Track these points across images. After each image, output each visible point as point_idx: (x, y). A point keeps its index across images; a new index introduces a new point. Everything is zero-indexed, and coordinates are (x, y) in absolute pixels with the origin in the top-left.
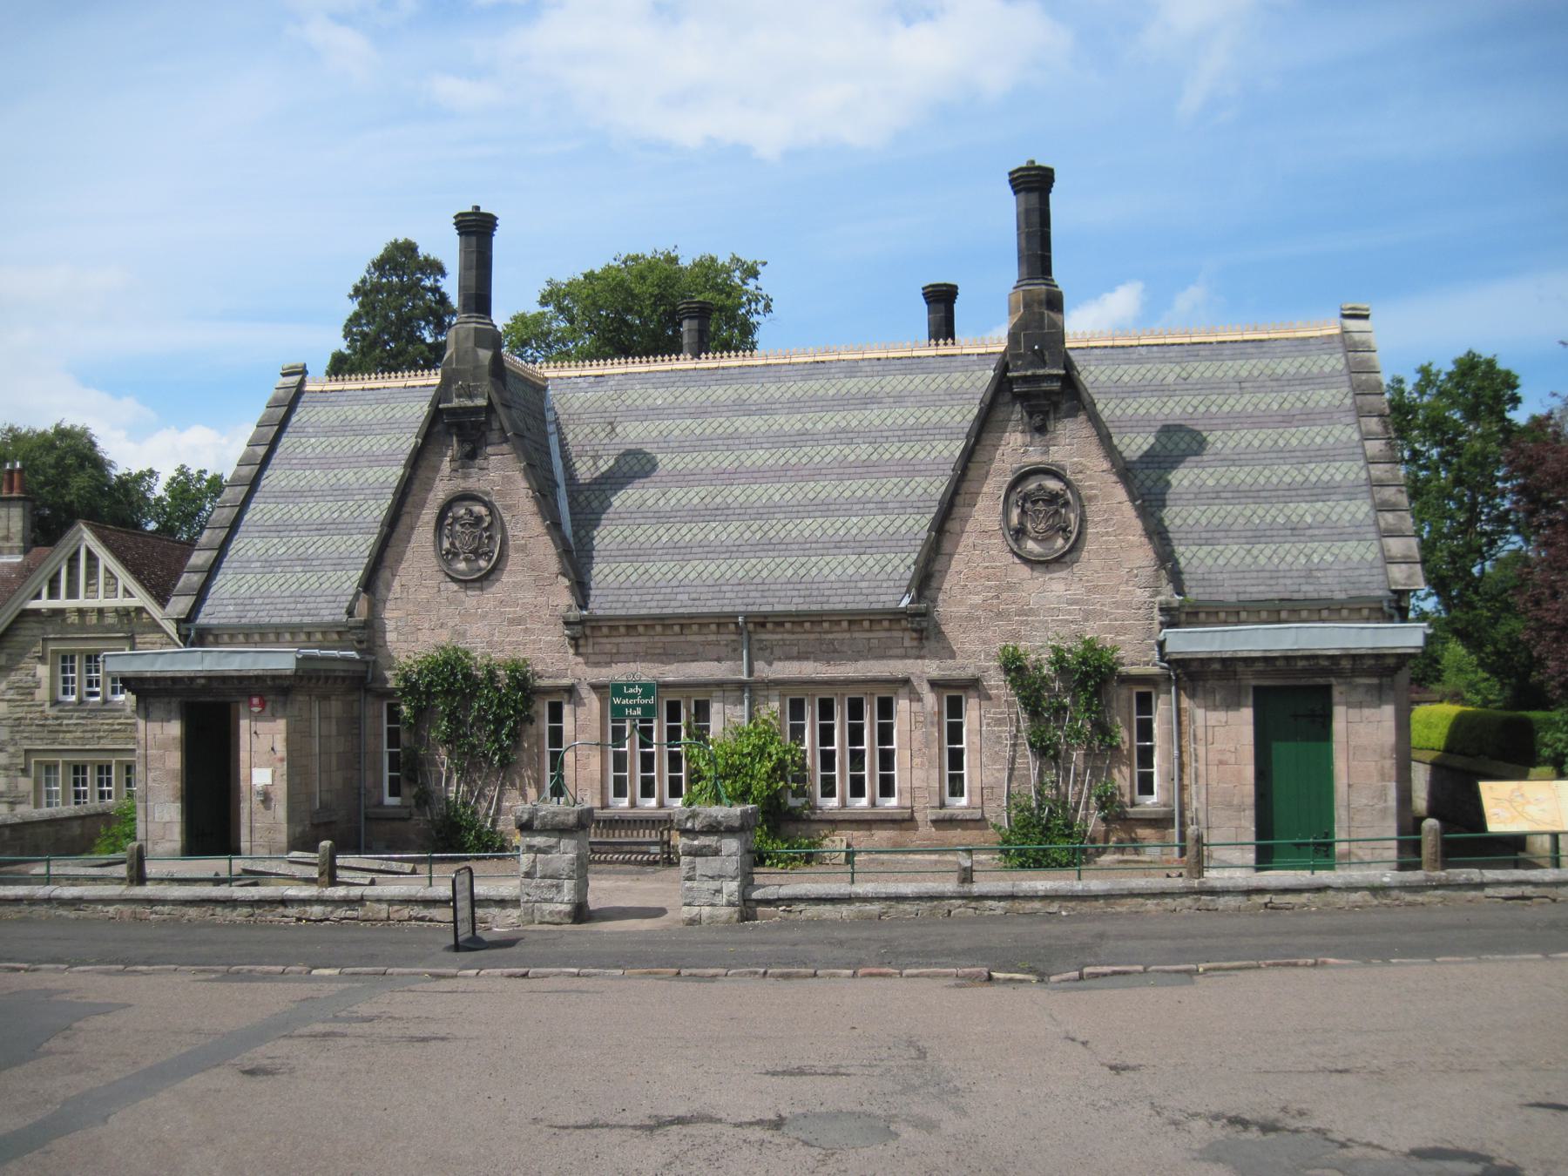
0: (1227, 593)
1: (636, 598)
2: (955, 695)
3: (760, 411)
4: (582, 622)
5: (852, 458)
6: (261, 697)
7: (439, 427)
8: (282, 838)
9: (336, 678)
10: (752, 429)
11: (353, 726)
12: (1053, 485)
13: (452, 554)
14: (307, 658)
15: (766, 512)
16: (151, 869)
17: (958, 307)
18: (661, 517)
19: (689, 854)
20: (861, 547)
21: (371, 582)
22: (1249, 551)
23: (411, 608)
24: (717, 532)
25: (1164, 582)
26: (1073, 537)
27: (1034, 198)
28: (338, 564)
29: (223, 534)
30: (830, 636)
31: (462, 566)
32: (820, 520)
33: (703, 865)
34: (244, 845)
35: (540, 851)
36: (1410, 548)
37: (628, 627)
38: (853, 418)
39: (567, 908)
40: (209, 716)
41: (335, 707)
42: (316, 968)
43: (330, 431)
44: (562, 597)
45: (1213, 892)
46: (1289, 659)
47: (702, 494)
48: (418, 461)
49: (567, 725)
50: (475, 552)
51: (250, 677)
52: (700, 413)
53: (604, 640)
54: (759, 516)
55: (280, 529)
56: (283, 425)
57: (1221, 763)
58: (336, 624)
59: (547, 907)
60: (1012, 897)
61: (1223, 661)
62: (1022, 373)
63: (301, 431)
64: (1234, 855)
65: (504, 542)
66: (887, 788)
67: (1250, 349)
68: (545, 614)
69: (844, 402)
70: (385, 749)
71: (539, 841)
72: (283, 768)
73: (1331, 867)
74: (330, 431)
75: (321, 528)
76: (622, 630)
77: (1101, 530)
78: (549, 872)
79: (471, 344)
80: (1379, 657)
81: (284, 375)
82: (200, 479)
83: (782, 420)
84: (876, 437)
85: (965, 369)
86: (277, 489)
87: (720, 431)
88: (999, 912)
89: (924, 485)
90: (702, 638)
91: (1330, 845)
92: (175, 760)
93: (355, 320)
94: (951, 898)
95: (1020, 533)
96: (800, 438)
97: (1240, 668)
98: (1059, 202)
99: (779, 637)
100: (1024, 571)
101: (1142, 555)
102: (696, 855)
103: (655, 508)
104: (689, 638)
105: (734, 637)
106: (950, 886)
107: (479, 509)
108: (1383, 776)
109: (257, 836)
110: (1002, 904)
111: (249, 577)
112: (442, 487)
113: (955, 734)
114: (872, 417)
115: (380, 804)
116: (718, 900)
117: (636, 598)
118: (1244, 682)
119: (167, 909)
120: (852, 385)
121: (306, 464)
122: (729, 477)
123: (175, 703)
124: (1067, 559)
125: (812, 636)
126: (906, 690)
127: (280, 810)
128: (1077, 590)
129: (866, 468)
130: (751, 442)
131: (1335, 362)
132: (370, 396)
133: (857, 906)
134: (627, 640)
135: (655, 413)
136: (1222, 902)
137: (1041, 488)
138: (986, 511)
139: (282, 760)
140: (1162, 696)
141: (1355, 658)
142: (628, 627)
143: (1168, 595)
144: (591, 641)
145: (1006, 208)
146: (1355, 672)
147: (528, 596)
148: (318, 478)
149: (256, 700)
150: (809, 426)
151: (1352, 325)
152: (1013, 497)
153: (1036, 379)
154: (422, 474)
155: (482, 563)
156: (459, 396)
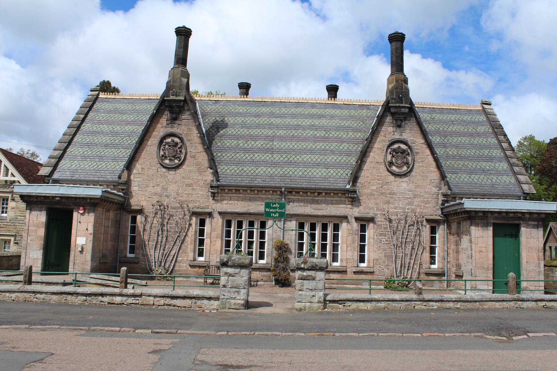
1: (240, 179)
2: (364, 223)
4: (218, 187)
5: (318, 135)
6: (83, 207)
7: (163, 107)
8: (88, 267)
9: (114, 202)
10: (278, 122)
11: (118, 223)
12: (403, 147)
13: (164, 157)
14: (106, 192)
16: (34, 278)
18: (246, 151)
19: (301, 279)
21: (129, 166)
22: (470, 177)
23: (145, 177)
25: (443, 185)
26: (411, 167)
27: (399, 44)
28: (115, 159)
29: (65, 145)
30: (317, 198)
31: (167, 161)
32: (310, 156)
34: (71, 270)
35: (231, 275)
36: (527, 179)
37: (236, 190)
38: (317, 122)
39: (243, 302)
40: (59, 215)
41: (112, 215)
42: (138, 329)
43: (110, 112)
44: (209, 176)
45: (523, 300)
46: (507, 213)
47: (262, 143)
48: (154, 119)
49: (207, 228)
50: (174, 157)
51: (80, 198)
52: (257, 116)
53: (225, 195)
54: (285, 153)
56: (91, 108)
57: (480, 251)
58: (113, 182)
59: (233, 301)
60: (442, 301)
62: (395, 105)
63: (98, 111)
65: (186, 154)
66: (335, 258)
68: (201, 183)
69: (312, 116)
70: (129, 234)
71: (230, 270)
72: (91, 237)
74: (110, 112)
75: (106, 146)
76: (234, 191)
77: (421, 165)
78: (235, 285)
79: (179, 76)
81: (91, 91)
82: (28, 153)
83: (289, 120)
84: (327, 129)
85: (355, 109)
86: (88, 130)
87: (266, 122)
88: (435, 307)
89: (347, 146)
90: (266, 196)
92: (42, 232)
94: (416, 301)
95: (391, 164)
96: (297, 127)
97: (489, 215)
99: (297, 197)
100: (392, 178)
101: (435, 175)
102: (304, 280)
103: (243, 147)
104: (260, 196)
105: (278, 197)
107: (177, 140)
109: (76, 267)
110: (437, 304)
111: (76, 162)
112: (160, 130)
113: (363, 238)
114: (323, 122)
115: (126, 256)
117: (240, 179)
118: (489, 221)
119: (42, 296)
120: (314, 111)
121: (100, 123)
122: (272, 138)
124: (408, 175)
125: (310, 198)
126: (346, 221)
127: (88, 255)
128: (412, 186)
129: (325, 139)
132: (126, 101)
133: (374, 304)
134: (235, 195)
136: (525, 305)
137: (399, 147)
138: (378, 154)
139: (91, 234)
140: (441, 226)
142: (236, 190)
143: (444, 189)
144: (220, 195)
146: (530, 219)
147: (195, 176)
148: (105, 128)
149: (81, 208)
150: (300, 123)
151: (486, 106)
152: (390, 150)
153: (399, 107)
154: (154, 124)
155: (176, 161)
156: (173, 95)
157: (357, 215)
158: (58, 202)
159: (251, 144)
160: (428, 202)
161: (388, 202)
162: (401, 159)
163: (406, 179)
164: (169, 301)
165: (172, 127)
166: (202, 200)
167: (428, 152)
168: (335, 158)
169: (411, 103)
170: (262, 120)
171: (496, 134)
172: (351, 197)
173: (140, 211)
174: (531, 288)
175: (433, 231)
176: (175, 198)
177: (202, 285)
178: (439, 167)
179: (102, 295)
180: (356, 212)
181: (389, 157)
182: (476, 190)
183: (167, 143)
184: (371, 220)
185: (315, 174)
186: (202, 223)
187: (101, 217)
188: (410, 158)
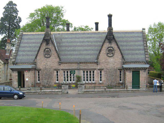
0: (129, 61)
2: (101, 70)
3: (78, 38)
12: (111, 49)
15: (80, 50)
17: (99, 25)
18: (68, 51)
20: (91, 55)
21: (36, 58)
24: (74, 53)
33: (81, 88)
38: (89, 40)
41: (33, 71)
43: (27, 39)
44: (58, 60)
45: (128, 90)
49: (59, 74)
52: (71, 38)
55: (24, 51)
60: (110, 91)
61: (129, 68)
63: (24, 39)
64: (130, 87)
67: (132, 33)
69: (88, 38)
71: (64, 86)
73: (139, 89)
74: (27, 39)
75: (29, 51)
77: (117, 54)
80: (144, 68)
84: (91, 42)
91: (139, 86)
92: (17, 78)
93: (4, 12)
95: (108, 54)
96: (83, 42)
98: (113, 18)
100: (108, 58)
101: (120, 56)
106: (104, 90)
107: (49, 50)
108: (145, 80)
113: (101, 75)
116: (82, 91)
120: (88, 36)
121: (25, 43)
122: (76, 46)
123: (17, 71)
129: (90, 46)
130: (77, 42)
131: (141, 35)
135: (66, 38)
138: (104, 51)
141: (142, 68)
145: (107, 19)
146: (142, 69)
151: (143, 30)
155: (49, 56)
157: (99, 68)
158: (20, 70)
159: (70, 48)
160: (119, 64)
161: (107, 65)
162: (110, 51)
163: (112, 58)
164: (51, 93)
165: (47, 46)
166: (56, 66)
167: (119, 50)
168: (93, 52)
169: (114, 36)
170: (73, 40)
171: (144, 41)
172: (97, 63)
173: (40, 70)
174: (142, 87)
175: (121, 72)
176: (49, 66)
177: (159, 91)
178: (122, 54)
179: (37, 92)
180: (99, 67)
181: (107, 52)
182: (133, 60)
183: (46, 51)
184: (103, 69)
185: (87, 57)
186: (57, 72)
187: (32, 74)
188: (113, 52)
